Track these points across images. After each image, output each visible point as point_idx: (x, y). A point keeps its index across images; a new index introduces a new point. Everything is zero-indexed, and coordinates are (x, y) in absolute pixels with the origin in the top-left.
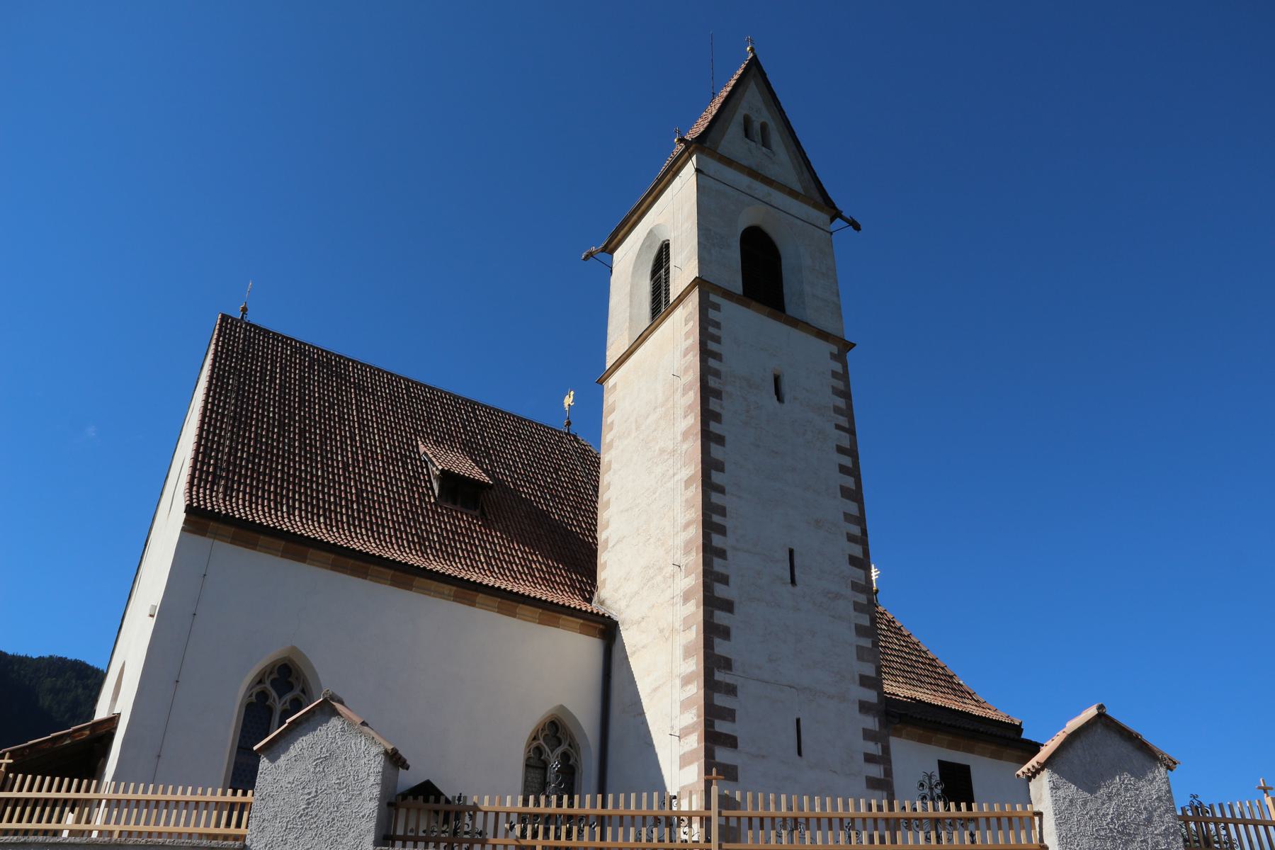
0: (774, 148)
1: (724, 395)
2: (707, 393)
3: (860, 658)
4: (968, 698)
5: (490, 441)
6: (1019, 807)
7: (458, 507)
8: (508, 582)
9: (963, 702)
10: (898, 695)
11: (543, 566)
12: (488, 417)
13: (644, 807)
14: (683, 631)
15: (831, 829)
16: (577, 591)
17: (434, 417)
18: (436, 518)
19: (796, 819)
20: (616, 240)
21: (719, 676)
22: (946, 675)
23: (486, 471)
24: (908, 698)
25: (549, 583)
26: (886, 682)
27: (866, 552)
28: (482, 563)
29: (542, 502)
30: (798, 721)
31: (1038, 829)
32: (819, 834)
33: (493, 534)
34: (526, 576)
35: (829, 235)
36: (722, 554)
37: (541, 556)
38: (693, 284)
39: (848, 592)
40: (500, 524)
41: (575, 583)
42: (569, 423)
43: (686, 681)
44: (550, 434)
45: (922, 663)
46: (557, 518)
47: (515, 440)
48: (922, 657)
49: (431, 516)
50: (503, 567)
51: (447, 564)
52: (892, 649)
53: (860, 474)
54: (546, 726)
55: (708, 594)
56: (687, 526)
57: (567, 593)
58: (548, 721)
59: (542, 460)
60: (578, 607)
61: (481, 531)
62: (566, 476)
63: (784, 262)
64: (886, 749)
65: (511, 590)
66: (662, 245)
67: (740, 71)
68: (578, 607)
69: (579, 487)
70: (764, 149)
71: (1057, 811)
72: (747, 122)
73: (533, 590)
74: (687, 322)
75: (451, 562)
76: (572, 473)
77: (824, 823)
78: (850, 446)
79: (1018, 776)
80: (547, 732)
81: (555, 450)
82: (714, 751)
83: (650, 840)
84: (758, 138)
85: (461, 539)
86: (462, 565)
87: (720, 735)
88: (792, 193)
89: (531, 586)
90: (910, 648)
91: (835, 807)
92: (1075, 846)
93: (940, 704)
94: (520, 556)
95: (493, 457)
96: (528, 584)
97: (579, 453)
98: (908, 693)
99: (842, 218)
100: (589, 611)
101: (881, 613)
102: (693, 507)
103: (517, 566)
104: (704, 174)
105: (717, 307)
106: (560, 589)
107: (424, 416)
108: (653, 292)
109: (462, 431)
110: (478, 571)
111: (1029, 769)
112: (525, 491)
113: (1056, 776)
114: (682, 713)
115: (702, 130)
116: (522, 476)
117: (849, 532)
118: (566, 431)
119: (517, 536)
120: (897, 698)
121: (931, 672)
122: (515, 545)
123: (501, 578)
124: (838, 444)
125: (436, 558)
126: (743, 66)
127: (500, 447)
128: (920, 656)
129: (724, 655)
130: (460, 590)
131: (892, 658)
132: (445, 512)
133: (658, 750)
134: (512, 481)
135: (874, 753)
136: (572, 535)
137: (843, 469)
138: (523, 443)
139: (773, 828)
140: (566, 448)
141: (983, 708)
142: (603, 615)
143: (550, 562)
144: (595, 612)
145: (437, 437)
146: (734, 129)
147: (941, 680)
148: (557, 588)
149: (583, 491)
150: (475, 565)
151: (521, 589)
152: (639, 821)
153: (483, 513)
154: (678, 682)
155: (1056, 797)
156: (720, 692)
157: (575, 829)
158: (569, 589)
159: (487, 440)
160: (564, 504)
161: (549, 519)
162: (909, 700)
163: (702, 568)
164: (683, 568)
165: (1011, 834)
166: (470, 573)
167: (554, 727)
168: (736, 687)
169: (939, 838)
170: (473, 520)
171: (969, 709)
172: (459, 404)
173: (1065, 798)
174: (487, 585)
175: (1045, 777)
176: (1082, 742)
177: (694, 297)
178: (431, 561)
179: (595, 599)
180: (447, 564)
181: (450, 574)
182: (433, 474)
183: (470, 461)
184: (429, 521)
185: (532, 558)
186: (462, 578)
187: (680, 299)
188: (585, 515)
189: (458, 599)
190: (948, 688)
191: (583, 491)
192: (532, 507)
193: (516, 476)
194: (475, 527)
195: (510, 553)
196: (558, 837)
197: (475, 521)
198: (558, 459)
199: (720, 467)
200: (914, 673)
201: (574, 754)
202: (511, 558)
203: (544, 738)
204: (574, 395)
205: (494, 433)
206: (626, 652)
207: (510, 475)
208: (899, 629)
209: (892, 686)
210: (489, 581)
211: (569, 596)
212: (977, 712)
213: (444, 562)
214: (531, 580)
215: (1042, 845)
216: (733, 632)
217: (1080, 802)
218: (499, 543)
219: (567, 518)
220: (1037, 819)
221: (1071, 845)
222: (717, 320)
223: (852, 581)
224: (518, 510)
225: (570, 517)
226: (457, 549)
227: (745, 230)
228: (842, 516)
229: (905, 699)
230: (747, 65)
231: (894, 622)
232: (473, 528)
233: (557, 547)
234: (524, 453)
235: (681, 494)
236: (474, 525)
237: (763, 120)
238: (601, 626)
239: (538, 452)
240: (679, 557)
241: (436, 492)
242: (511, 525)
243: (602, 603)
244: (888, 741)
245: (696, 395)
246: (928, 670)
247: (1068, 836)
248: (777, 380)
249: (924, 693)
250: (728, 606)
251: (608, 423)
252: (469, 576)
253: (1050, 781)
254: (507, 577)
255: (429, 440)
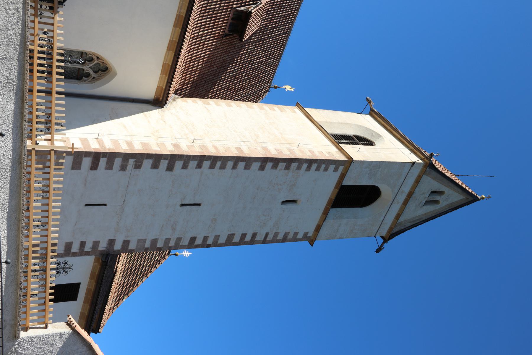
0: (425, 207)
1: (287, 171)
2: (289, 162)
3: (139, 241)
4: (115, 303)
5: (267, 42)
6: (51, 315)
7: (230, 21)
8: (187, 47)
9: (113, 300)
10: (118, 263)
11: (196, 68)
12: (281, 42)
13: (57, 108)
14: (157, 143)
15: (42, 211)
16: (181, 86)
17: (282, 10)
18: (224, 8)
19: (48, 192)
20: (377, 117)
21: (131, 162)
22: (128, 291)
23: (250, 38)
24: (116, 269)
25: (186, 70)
26: (126, 255)
27: (197, 246)
28: (198, 33)
29: (232, 70)
30: (105, 205)
31: (37, 326)
32: (40, 204)
33: (215, 41)
34: (190, 58)
35: (374, 235)
36: (199, 166)
37: (201, 67)
38: (350, 157)
39: (176, 236)
40: (220, 45)
41: (186, 86)
42: (276, 88)
43: (129, 144)
44: (270, 77)
45: (136, 278)
46: (222, 78)
47: (267, 56)
48: (139, 279)
49: (226, 4)
50: (196, 45)
51: (198, 12)
52: (144, 262)
53: (240, 245)
54: (106, 65)
55: (177, 157)
56: (215, 147)
57: (180, 81)
58: (108, 66)
59: (255, 71)
60: (172, 86)
61: (216, 33)
62: (246, 84)
63: (359, 209)
64: (87, 254)
65: (182, 48)
66: (372, 142)
67: (470, 191)
68: (172, 86)
69: (240, 91)
70: (424, 201)
71: (47, 336)
72: (440, 193)
73: (182, 61)
74: (328, 153)
75: (199, 14)
76: (248, 88)
77: (46, 208)
78: (257, 241)
79: (69, 316)
80: (102, 65)
81: (261, 79)
82: (89, 157)
83: (37, 110)
84: (431, 198)
85: (212, 22)
86: (197, 21)
87: (98, 160)
88: (398, 216)
89: (185, 60)
90: (144, 272)
91: (54, 214)
92: (27, 346)
93: (112, 287)
94: (202, 55)
95: (258, 43)
96: (185, 59)
97: (259, 92)
98: (119, 269)
99: (384, 243)
100: (170, 92)
101: (164, 257)
102: (226, 151)
103: (196, 53)
104: (411, 167)
105: (336, 170)
106: (183, 77)
107: (282, 4)
108: (347, 136)
109: (273, 26)
110: (193, 30)
111: (72, 321)
112: (238, 60)
113: (67, 336)
114: (111, 140)
115: (437, 167)
116: (246, 59)
117: (209, 237)
118: (271, 86)
119: (213, 54)
120: (117, 263)
121: (131, 283)
122: (208, 53)
123: (189, 43)
124: (258, 234)
125: (202, 6)
126: (473, 193)
127: (264, 47)
128: (140, 277)
129: (143, 165)
130: (183, 19)
131: (139, 262)
132: (228, 13)
133: (90, 126)
134: (244, 53)
135: (85, 247)
136: (212, 86)
137: (244, 236)
138: (265, 61)
139: (43, 179)
140: (262, 85)
141: (109, 312)
142: (167, 100)
143: (198, 72)
144: (169, 95)
145: (271, 11)
146: (437, 185)
147: (126, 289)
148: (183, 75)
149: (237, 93)
150: (197, 29)
151: (183, 54)
152: (49, 105)
153: (226, 35)
154: (129, 139)
155: (56, 336)
156: (122, 162)
157: (44, 69)
158: (182, 82)
159: (268, 40)
160: (231, 82)
161: (222, 73)
162: (115, 269)
163: (192, 154)
164: (192, 144)
165: (36, 311)
166: (192, 25)
167: (104, 69)
168: (124, 171)
169: (35, 271)
170: (223, 29)
171: (109, 303)
172: (289, 25)
173: (55, 341)
174: (186, 34)
175: (66, 330)
176: (86, 351)
177: (342, 158)
178: (200, 3)
179: (177, 96)
180: (198, 12)
181: (192, 13)
182: (249, 7)
183: (256, 30)
184: (223, 4)
185: (201, 62)
186: (190, 20)
187: (341, 150)
188: (224, 94)
189: (178, 17)
190: (121, 292)
191: (237, 93)
192: (229, 64)
193: (247, 56)
194: (219, 30)
195: (204, 49)
196: (39, 58)
197: (222, 30)
198: (256, 80)
199: (247, 167)
200: (130, 273)
201: (89, 80)
202: (201, 50)
203: (98, 63)
204: (291, 91)
205: (271, 45)
206: (146, 112)
207: (247, 52)
208: (155, 267)
209: (124, 260)
210: (188, 36)
211: (178, 82)
212: (107, 308)
213: (199, 10)
214: (188, 60)
215: (29, 328)
216: (155, 171)
217: (52, 349)
218: (209, 43)
219: (223, 83)
220: (44, 326)
221: (28, 344)
222: (329, 169)
223: (182, 238)
224: (228, 56)
225: (223, 85)
226: (206, 19)
227: (377, 187)
228: (218, 234)
229: (116, 267)
230: (474, 195)
231: (159, 264)
232: (218, 29)
233: (206, 77)
234: (260, 61)
235: (233, 145)
236: (220, 30)
237: (441, 202)
238: (161, 98)
239: (260, 69)
240: (197, 143)
241: (239, 9)
242: (219, 51)
243: (174, 100)
244: (92, 255)
245: (287, 156)
246: (132, 282)
247: (33, 343)
248: (294, 201)
249: (119, 279)
250: (170, 168)
251: (274, 108)
252: (191, 24)
253: (65, 332)
254: (190, 47)
255: (269, 6)
